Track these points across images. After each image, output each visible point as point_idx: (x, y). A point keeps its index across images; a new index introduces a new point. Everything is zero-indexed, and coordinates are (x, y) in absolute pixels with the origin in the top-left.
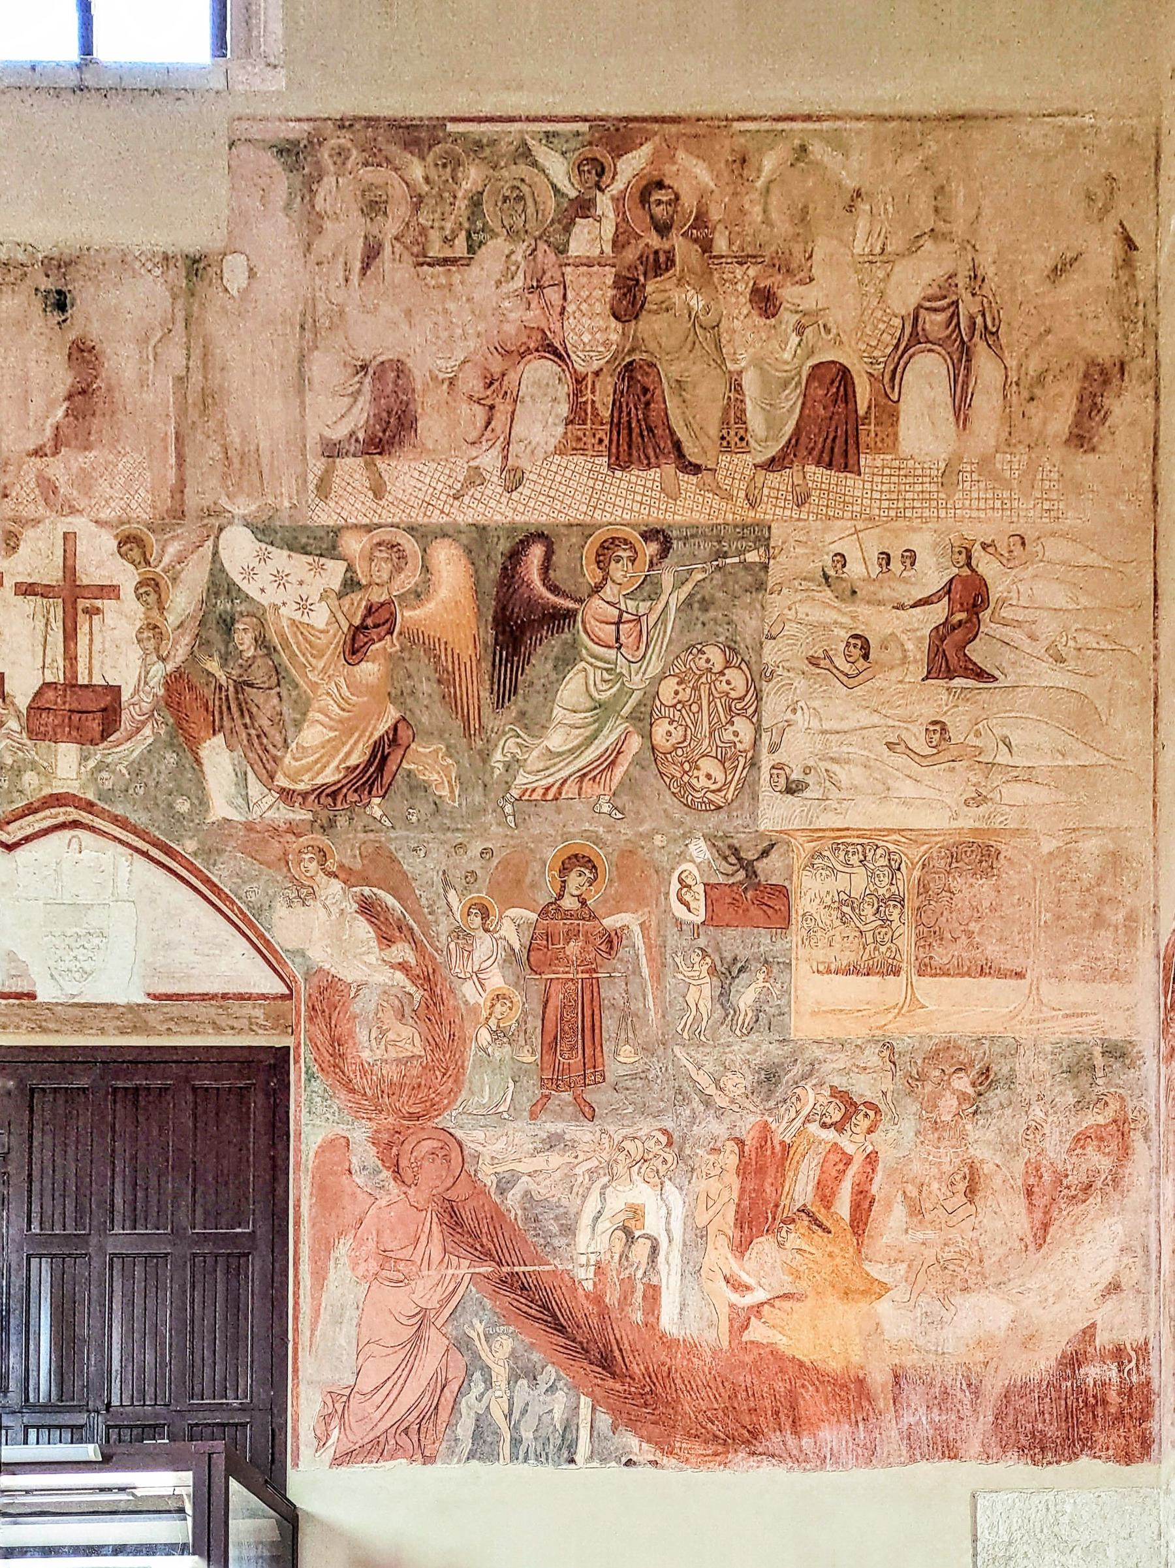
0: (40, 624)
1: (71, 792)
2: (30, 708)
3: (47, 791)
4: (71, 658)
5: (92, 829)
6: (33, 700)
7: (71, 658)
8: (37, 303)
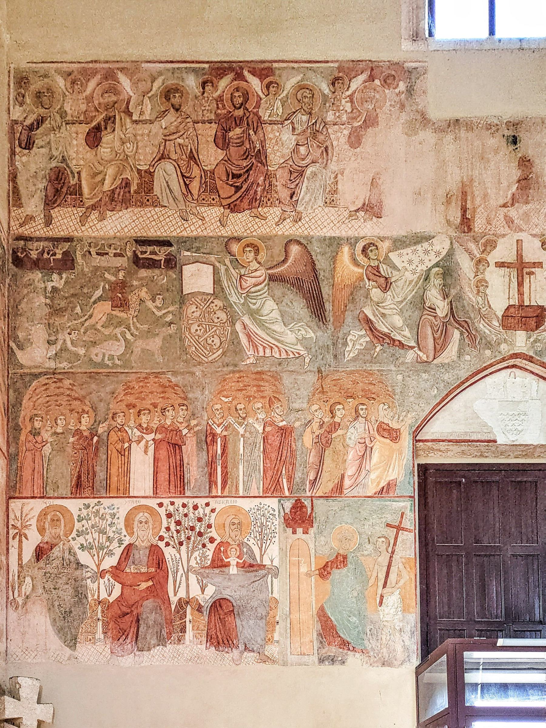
0: (507, 279)
1: (523, 352)
2: (503, 316)
3: (511, 352)
4: (521, 294)
5: (521, 368)
6: (505, 312)
7: (521, 294)
8: (504, 142)
